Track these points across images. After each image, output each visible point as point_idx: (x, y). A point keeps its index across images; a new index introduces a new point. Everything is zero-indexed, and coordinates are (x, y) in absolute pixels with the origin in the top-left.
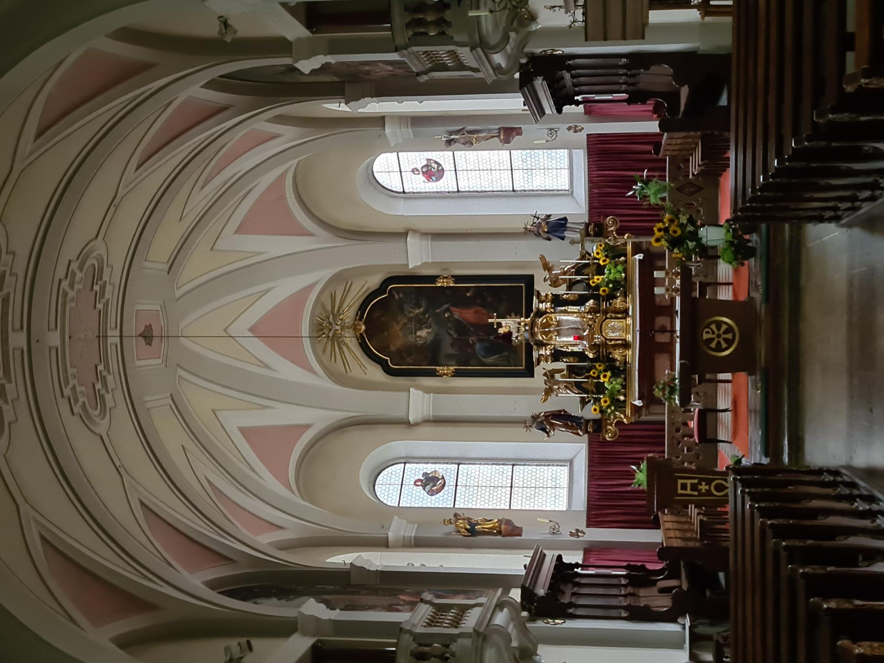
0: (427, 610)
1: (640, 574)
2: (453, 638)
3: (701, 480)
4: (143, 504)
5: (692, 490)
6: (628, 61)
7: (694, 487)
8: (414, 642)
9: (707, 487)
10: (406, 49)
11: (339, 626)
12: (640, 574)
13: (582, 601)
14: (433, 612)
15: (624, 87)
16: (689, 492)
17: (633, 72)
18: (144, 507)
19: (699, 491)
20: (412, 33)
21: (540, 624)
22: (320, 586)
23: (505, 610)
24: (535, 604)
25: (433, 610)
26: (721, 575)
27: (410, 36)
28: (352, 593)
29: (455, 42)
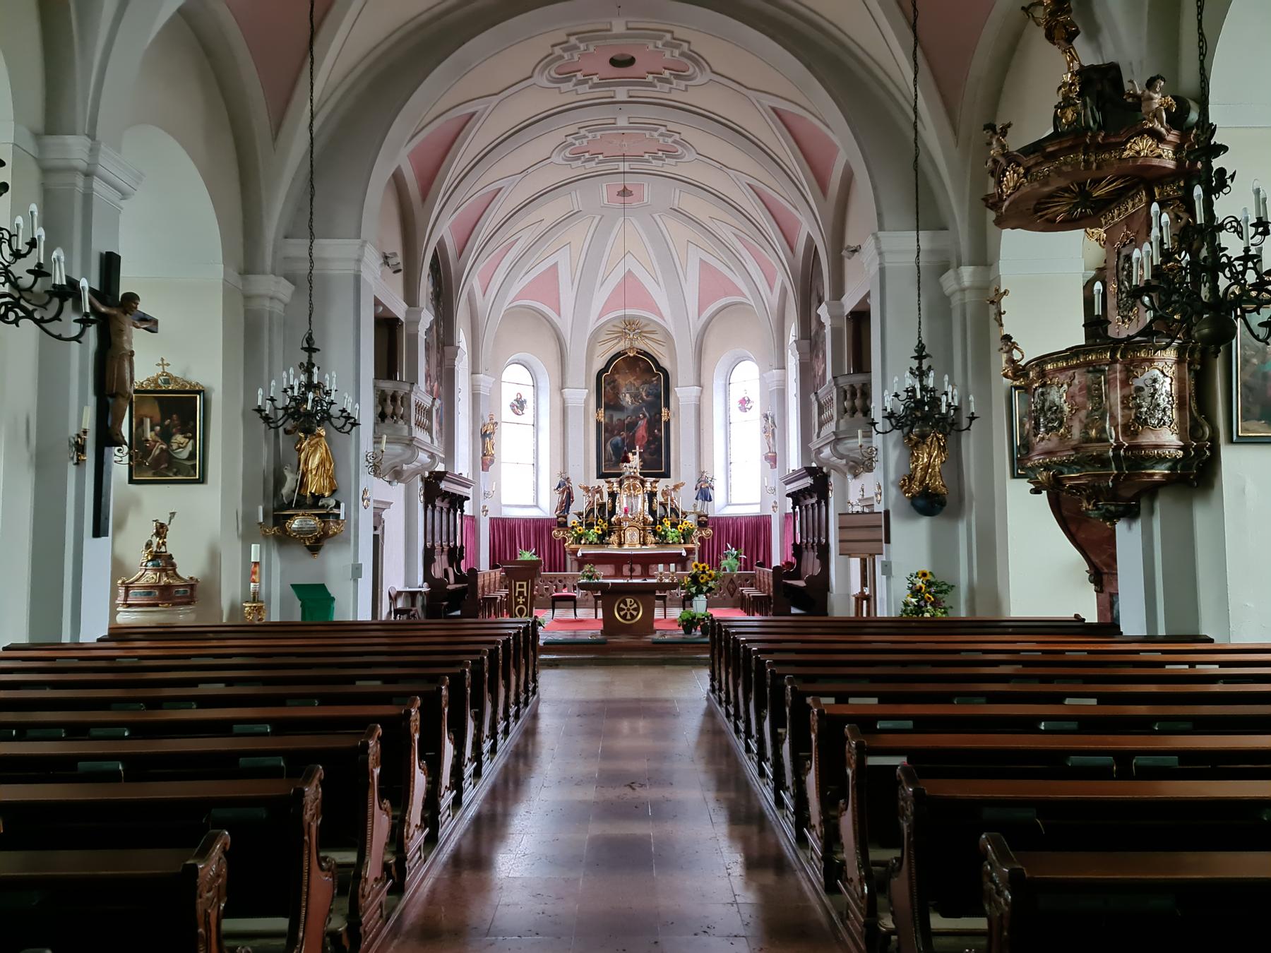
2: (408, 422)
5: (519, 592)
7: (521, 593)
9: (521, 602)
11: (413, 338)
16: (518, 590)
18: (496, 191)
21: (420, 485)
28: (438, 348)
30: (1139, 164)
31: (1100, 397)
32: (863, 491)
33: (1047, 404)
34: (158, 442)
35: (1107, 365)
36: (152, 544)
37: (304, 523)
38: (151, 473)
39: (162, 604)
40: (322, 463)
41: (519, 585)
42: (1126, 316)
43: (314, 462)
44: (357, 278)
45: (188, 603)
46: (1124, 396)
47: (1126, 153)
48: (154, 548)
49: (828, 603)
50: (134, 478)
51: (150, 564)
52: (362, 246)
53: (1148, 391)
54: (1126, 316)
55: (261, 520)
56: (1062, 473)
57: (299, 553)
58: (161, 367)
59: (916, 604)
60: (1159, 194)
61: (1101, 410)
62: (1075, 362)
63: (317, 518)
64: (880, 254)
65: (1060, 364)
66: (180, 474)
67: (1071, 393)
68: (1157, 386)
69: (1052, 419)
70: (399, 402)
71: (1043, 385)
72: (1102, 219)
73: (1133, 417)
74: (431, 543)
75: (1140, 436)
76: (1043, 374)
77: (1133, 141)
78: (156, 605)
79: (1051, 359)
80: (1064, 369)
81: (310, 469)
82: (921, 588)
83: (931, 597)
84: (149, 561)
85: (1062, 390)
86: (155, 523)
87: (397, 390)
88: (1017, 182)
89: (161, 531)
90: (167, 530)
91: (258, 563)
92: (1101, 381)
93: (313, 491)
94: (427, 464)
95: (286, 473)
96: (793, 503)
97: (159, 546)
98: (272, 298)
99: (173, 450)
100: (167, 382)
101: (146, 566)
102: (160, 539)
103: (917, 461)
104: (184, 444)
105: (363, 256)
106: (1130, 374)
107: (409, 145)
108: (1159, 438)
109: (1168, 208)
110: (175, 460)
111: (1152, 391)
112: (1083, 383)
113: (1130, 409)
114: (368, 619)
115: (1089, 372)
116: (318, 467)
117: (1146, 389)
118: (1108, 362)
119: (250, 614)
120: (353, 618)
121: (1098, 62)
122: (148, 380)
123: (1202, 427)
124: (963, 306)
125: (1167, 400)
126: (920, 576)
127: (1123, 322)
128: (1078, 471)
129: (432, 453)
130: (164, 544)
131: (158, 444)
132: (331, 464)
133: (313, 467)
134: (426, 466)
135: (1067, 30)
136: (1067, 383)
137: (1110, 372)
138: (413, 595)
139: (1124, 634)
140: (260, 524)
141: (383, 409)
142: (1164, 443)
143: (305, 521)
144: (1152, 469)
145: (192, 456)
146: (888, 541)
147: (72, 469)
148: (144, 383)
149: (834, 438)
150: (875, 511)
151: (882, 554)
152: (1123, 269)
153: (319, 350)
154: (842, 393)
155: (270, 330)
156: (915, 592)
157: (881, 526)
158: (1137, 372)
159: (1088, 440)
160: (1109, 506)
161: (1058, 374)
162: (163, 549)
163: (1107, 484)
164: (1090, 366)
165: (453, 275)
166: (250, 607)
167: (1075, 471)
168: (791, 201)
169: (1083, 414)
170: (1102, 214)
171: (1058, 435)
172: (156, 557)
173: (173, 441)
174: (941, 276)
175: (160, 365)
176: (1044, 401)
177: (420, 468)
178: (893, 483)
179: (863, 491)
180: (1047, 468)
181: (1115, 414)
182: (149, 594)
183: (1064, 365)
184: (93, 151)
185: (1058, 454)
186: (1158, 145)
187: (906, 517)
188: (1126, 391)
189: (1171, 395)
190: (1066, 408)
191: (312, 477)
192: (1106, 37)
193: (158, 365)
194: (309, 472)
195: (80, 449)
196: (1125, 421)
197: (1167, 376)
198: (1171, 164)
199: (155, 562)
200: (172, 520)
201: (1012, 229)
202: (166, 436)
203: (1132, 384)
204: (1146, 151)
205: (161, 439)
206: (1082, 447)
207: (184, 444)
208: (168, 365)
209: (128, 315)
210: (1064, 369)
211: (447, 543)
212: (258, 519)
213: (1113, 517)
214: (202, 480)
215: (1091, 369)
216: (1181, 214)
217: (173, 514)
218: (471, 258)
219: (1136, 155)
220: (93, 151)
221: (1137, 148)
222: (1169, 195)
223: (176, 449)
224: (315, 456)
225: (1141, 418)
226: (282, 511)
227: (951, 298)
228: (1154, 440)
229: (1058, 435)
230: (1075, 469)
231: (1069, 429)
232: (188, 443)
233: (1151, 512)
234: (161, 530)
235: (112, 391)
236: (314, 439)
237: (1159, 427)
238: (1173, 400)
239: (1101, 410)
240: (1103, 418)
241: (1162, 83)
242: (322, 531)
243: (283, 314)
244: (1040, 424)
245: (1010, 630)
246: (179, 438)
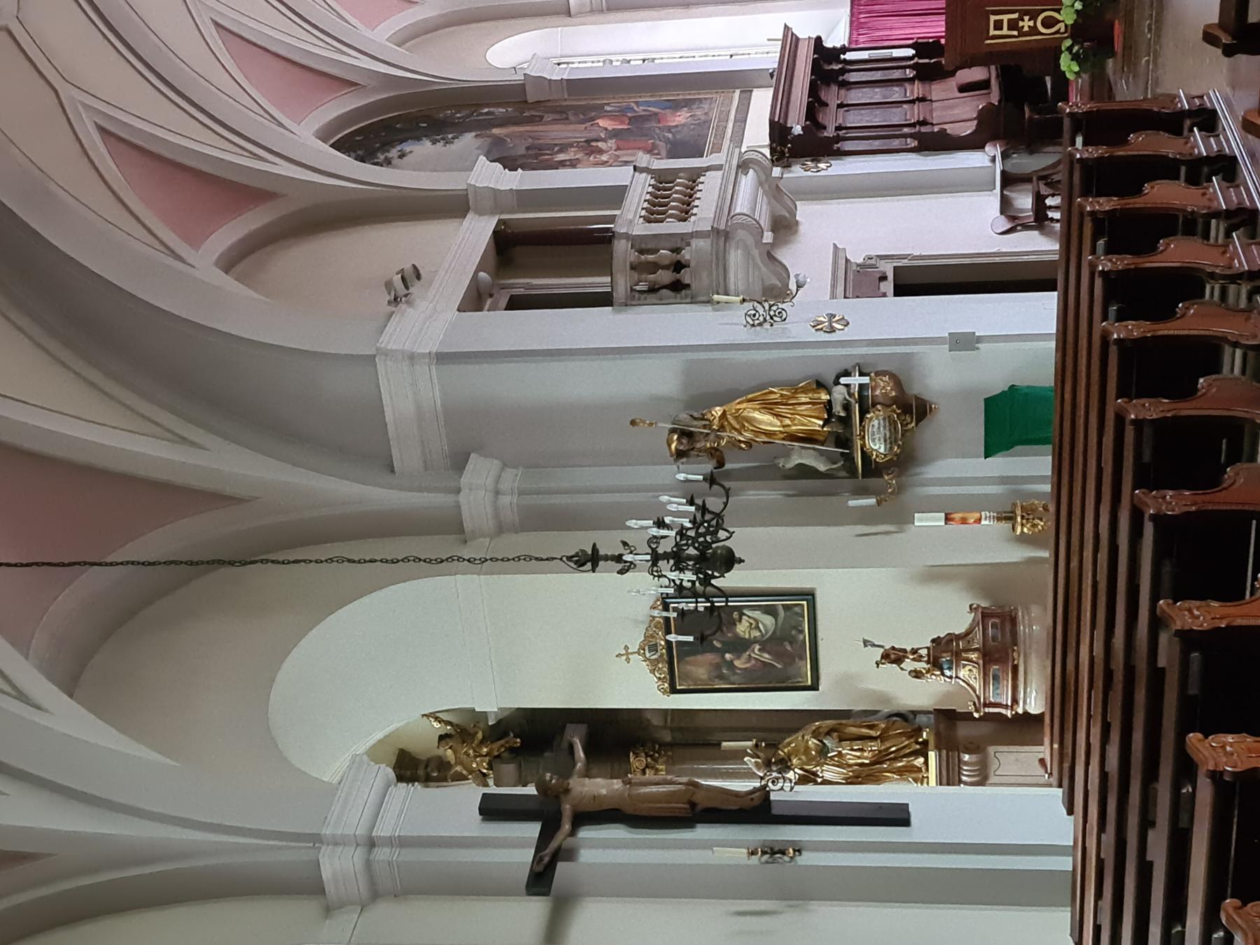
0: (646, 179)
1: (933, 61)
2: (686, 239)
3: (1023, 14)
4: (217, 24)
5: (1009, 29)
7: (1013, 25)
8: (633, 250)
9: (1031, 23)
11: (526, 198)
12: (933, 61)
14: (653, 186)
16: (1005, 31)
18: (220, 29)
19: (1020, 29)
21: (797, 171)
22: (486, 110)
23: (751, 171)
24: (789, 145)
25: (653, 182)
26: (1048, 80)
28: (531, 120)
34: (750, 655)
36: (915, 671)
37: (877, 436)
38: (801, 663)
39: (1014, 660)
40: (768, 407)
41: (995, 29)
43: (766, 420)
44: (442, 358)
45: (1014, 621)
48: (921, 666)
50: (809, 683)
51: (947, 673)
52: (386, 353)
55: (872, 501)
57: (928, 433)
58: (630, 657)
63: (868, 416)
66: (801, 626)
70: (651, 257)
74: (909, 140)
78: (1015, 669)
81: (781, 429)
84: (943, 674)
86: (881, 665)
87: (628, 264)
89: (894, 656)
90: (893, 648)
91: (946, 515)
93: (821, 423)
94: (758, 177)
95: (790, 465)
97: (919, 659)
98: (497, 493)
99: (762, 636)
100: (654, 648)
101: (951, 677)
102: (908, 658)
104: (752, 621)
105: (403, 352)
107: (190, 261)
110: (778, 633)
114: (1061, 795)
116: (777, 415)
119: (1034, 526)
120: (1051, 340)
122: (652, 671)
129: (739, 167)
130: (914, 651)
131: (753, 655)
132: (772, 392)
133: (779, 424)
134: (763, 177)
138: (1009, 180)
140: (879, 503)
141: (665, 287)
143: (873, 434)
145: (770, 611)
147: (806, 859)
148: (658, 675)
153: (594, 545)
155: (550, 492)
162: (924, 652)
165: (392, 94)
166: (1022, 525)
172: (936, 664)
173: (747, 636)
175: (627, 651)
177: (766, 187)
182: (996, 678)
184: (336, 842)
191: (795, 425)
193: (628, 660)
194: (787, 429)
195: (774, 851)
199: (945, 666)
200: (876, 643)
202: (740, 646)
205: (746, 651)
207: (752, 621)
208: (626, 648)
209: (570, 787)
211: (907, 85)
212: (871, 506)
214: (809, 596)
217: (866, 643)
218: (355, 62)
220: (336, 842)
223: (760, 631)
224: (755, 419)
226: (856, 468)
232: (748, 616)
234: (893, 656)
235: (685, 809)
236: (730, 423)
242: (890, 406)
243: (521, 469)
246: (742, 629)
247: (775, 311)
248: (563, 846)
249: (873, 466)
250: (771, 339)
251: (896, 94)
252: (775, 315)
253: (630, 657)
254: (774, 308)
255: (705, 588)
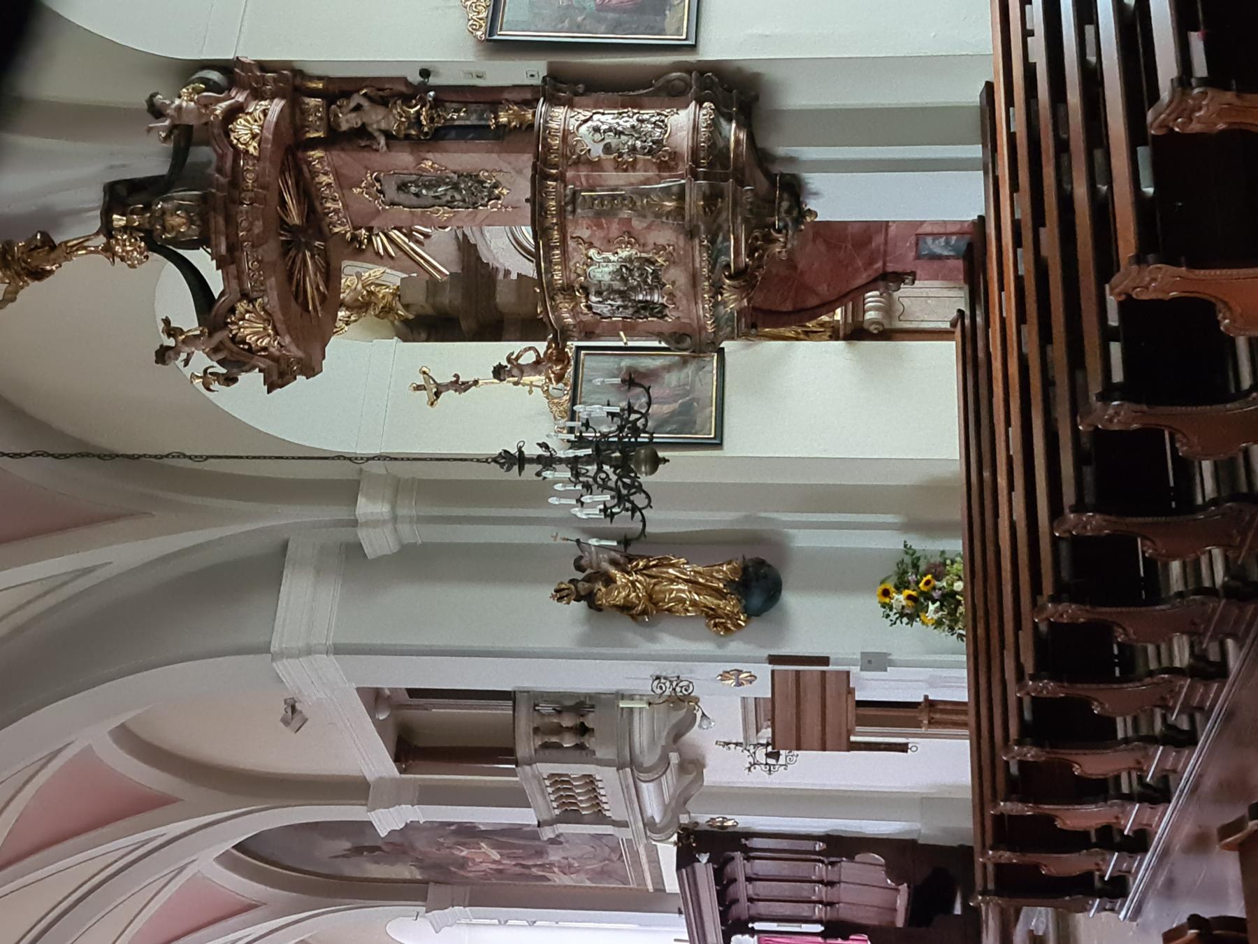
6: (825, 847)
10: (530, 764)
13: (762, 907)
15: (819, 911)
17: (832, 859)
20: (540, 743)
27: (537, 746)
29: (597, 759)
30: (271, 137)
31: (614, 197)
32: (729, 744)
33: (617, 285)
35: (566, 186)
42: (491, 193)
46: (615, 169)
47: (251, 150)
49: (942, 844)
53: (611, 139)
54: (491, 193)
56: (728, 266)
58: (533, 388)
59: (938, 604)
60: (317, 131)
61: (634, 197)
62: (556, 232)
64: (309, 651)
65: (556, 258)
67: (602, 245)
68: (604, 127)
69: (641, 275)
71: (586, 290)
72: (336, 230)
73: (649, 157)
75: (678, 150)
76: (568, 289)
77: (235, 141)
79: (546, 272)
80: (564, 253)
82: (909, 597)
83: (925, 579)
85: (596, 257)
88: (259, 316)
92: (591, 196)
96: (743, 933)
103: (682, 601)
106: (582, 158)
108: (682, 127)
109: (341, 120)
111: (612, 134)
112: (589, 222)
113: (635, 160)
115: (574, 212)
117: (607, 141)
118: (562, 185)
121: (94, 218)
123: (669, 81)
124: (423, 520)
125: (627, 119)
126: (887, 600)
127: (498, 198)
128: (727, 239)
135: (37, 247)
136: (586, 249)
137: (578, 184)
139: (983, 213)
142: (692, 122)
144: (729, 140)
146: (824, 661)
149: (628, 770)
150: (770, 696)
151: (848, 673)
152: (417, 195)
154: (547, 752)
156: (912, 613)
157: (798, 672)
158: (582, 151)
159: (679, 211)
160: (782, 210)
161: (572, 263)
163: (749, 192)
164: (565, 211)
167: (725, 244)
168: (168, 877)
169: (637, 224)
170: (326, 229)
171: (668, 267)
174: (365, 555)
176: (611, 290)
178: (720, 646)
179: (729, 744)
180: (717, 289)
181: (642, 178)
183: (558, 252)
185: (698, 265)
186: (247, 114)
187: (782, 625)
188: (609, 165)
189: (620, 114)
190: (624, 253)
192: (62, 200)
196: (654, 167)
197: (591, 117)
198: (276, 106)
201: (324, 358)
203: (599, 157)
204: (254, 127)
206: (690, 221)
210: (564, 253)
213: (799, 213)
215: (569, 208)
216: (352, 104)
219: (258, 138)
221: (247, 138)
222: (320, 119)
225: (651, 146)
227: (406, 542)
228: (685, 133)
229: (668, 267)
230: (722, 242)
231: (658, 248)
233: (791, 160)
237: (666, 126)
238: (627, 113)
239: (634, 199)
240: (646, 194)
241: (159, 96)
244: (647, 301)
245: (986, 474)
247: (664, 684)
248: (627, 387)
249: (622, 333)
250: (517, 912)
251: (802, 869)
252: (659, 683)
253: (533, 388)
254: (668, 684)
255: (342, 304)
